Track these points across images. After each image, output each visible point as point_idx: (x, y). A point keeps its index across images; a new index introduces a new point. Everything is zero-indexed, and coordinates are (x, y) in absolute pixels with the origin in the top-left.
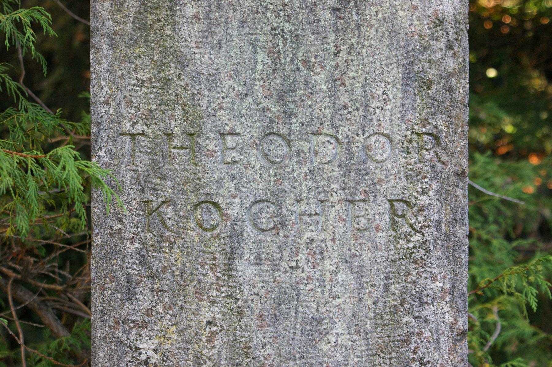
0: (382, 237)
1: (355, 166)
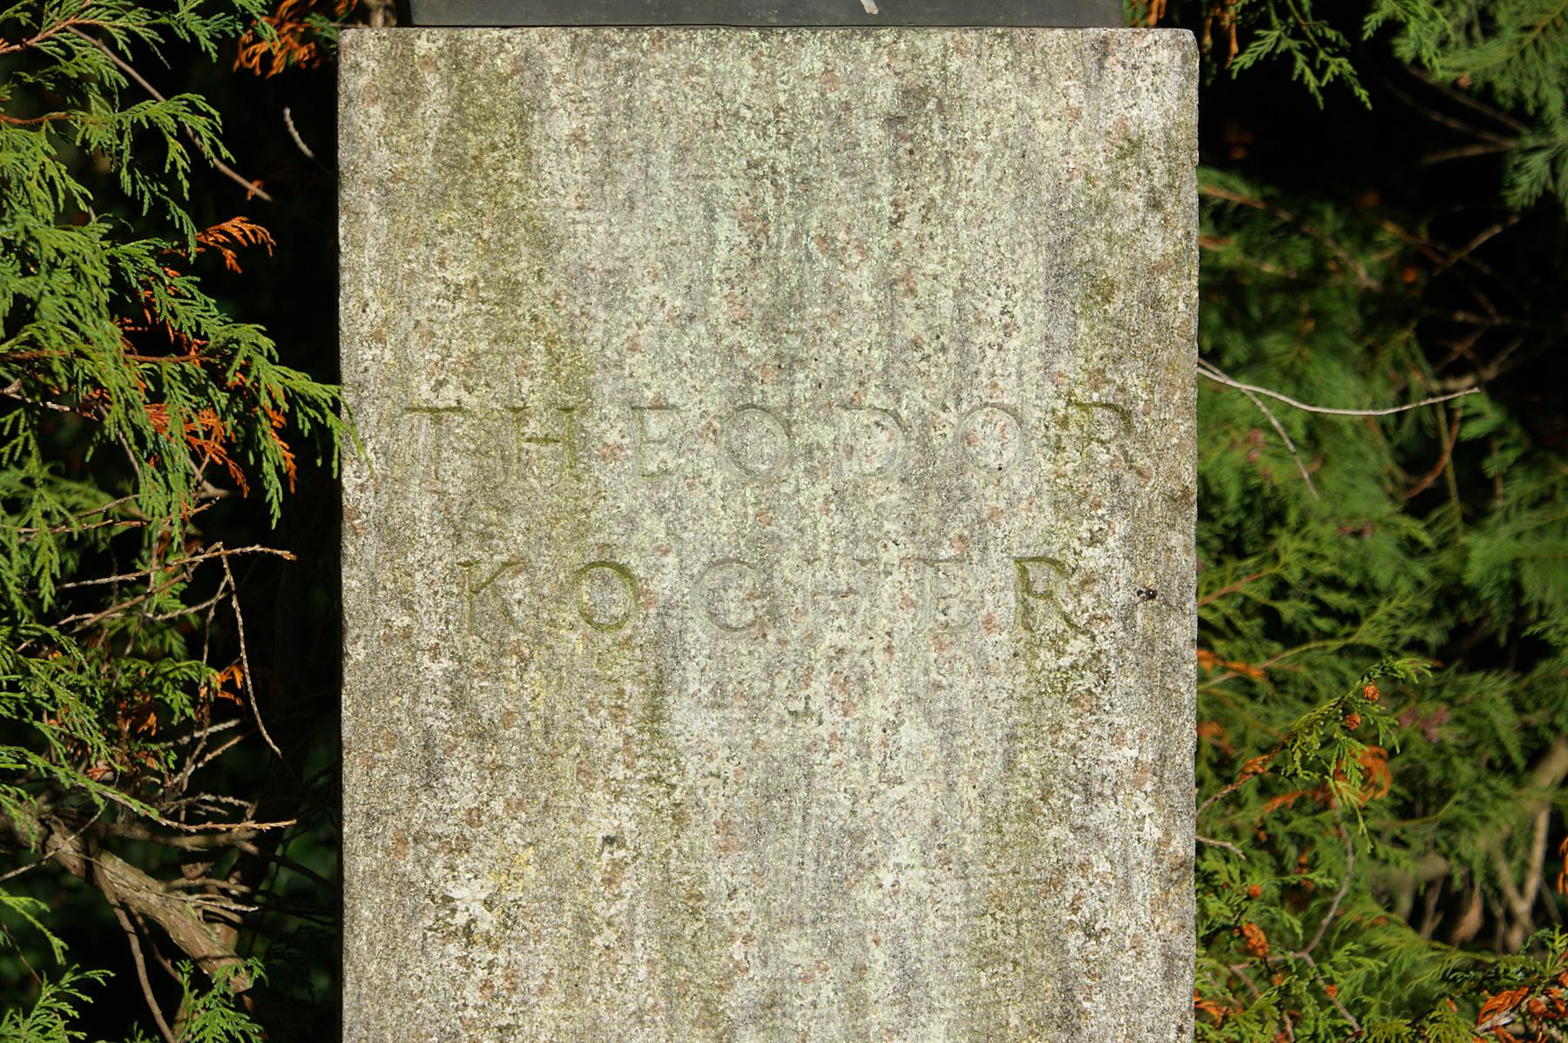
1: (939, 481)
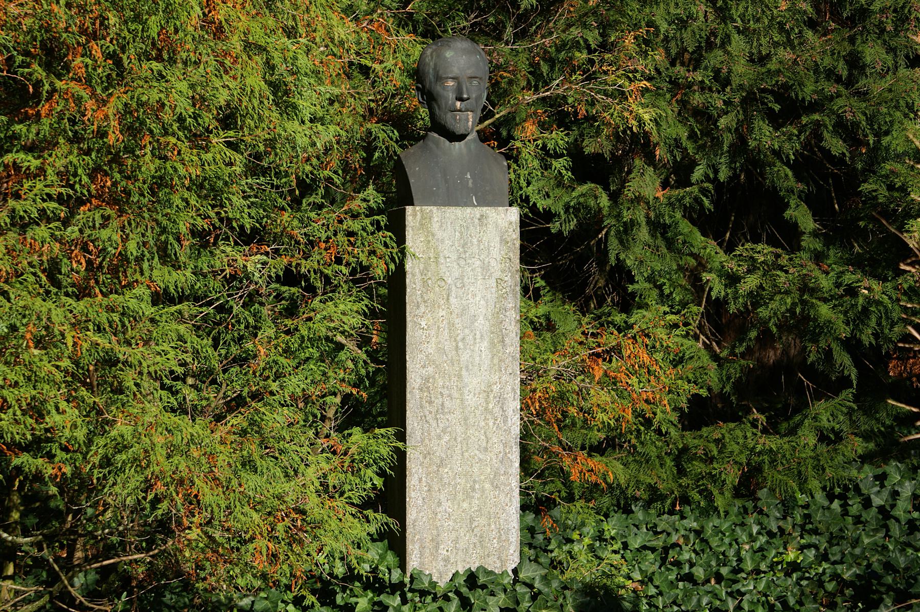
0: (494, 290)
1: (485, 268)
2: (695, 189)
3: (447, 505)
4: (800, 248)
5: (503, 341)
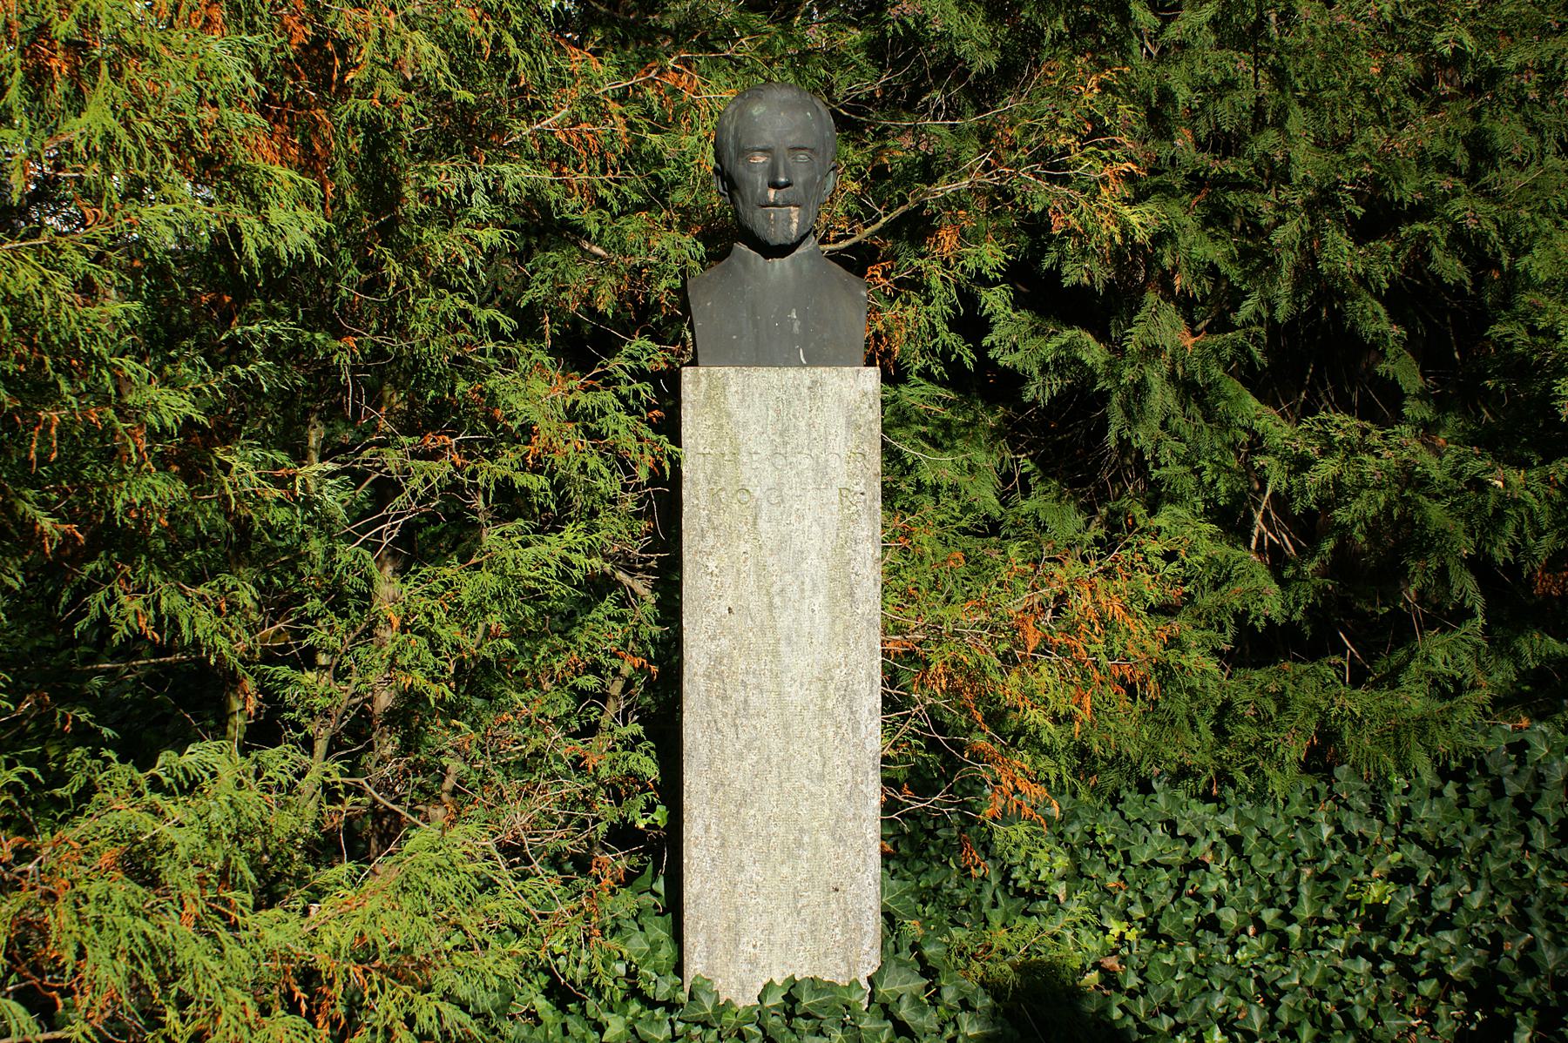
0: (835, 508)
1: (821, 470)
2: (1239, 336)
3: (752, 870)
4: (1400, 418)
5: (852, 594)
